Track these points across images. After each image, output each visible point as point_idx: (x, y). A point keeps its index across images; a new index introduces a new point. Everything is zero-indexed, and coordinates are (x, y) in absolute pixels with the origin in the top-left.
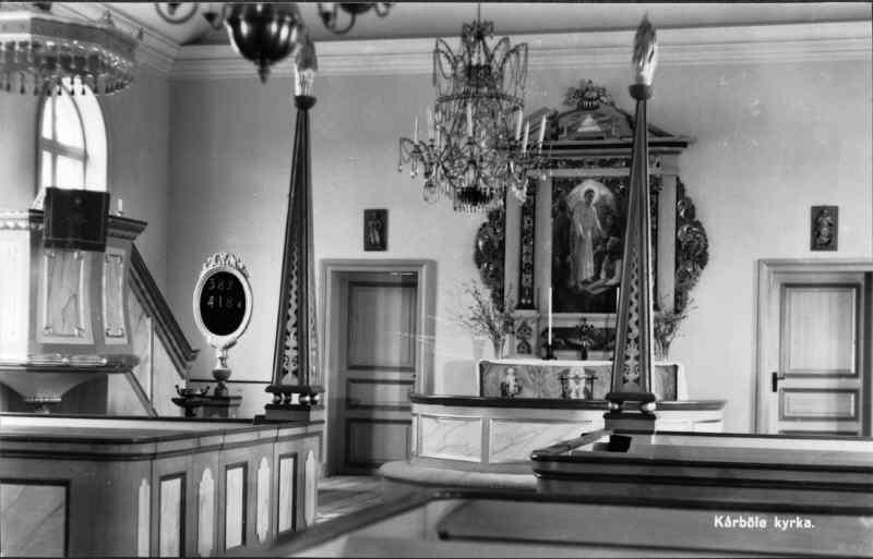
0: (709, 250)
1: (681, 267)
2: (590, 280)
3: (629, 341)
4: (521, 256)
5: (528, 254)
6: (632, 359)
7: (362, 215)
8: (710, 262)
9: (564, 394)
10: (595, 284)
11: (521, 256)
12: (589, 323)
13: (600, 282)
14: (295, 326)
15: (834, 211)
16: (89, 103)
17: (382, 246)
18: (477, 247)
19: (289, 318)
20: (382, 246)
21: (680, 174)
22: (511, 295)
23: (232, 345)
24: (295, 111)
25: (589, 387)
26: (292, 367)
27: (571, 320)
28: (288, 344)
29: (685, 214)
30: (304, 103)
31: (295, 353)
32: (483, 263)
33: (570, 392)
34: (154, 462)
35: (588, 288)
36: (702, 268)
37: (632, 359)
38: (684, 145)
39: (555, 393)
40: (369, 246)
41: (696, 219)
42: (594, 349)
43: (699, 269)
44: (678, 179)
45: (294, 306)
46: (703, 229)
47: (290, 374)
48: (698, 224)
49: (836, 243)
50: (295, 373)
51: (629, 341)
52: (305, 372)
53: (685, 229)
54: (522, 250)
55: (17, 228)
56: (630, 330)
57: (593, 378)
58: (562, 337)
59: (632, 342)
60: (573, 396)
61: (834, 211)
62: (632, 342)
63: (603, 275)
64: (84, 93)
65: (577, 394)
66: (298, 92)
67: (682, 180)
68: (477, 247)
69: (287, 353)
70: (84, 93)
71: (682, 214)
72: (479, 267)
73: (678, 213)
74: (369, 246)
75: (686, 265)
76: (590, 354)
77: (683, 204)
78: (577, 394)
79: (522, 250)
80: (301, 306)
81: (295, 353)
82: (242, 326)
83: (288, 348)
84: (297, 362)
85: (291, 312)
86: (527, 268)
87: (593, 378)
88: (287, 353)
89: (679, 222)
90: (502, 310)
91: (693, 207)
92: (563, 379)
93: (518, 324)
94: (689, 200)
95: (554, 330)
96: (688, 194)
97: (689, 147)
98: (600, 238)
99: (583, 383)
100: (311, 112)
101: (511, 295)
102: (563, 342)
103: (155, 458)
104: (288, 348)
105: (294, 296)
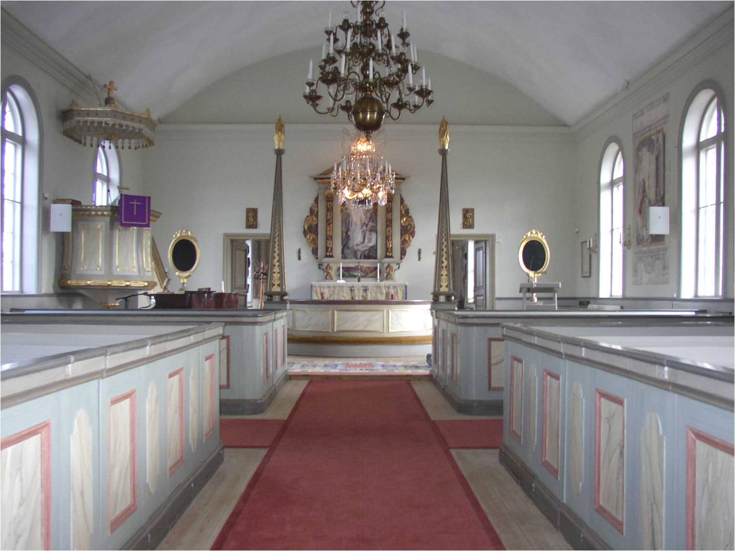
0: (415, 229)
1: (403, 237)
2: (360, 244)
3: (442, 267)
4: (327, 232)
5: (329, 231)
6: (444, 276)
7: (244, 213)
8: (416, 235)
9: (352, 298)
10: (362, 245)
11: (327, 232)
12: (361, 264)
13: (365, 244)
14: (278, 261)
15: (472, 210)
16: (112, 153)
17: (471, 226)
18: (304, 227)
19: (445, 246)
20: (471, 226)
21: (402, 194)
22: (321, 251)
23: (189, 276)
24: (275, 156)
25: (364, 294)
26: (277, 282)
27: (352, 263)
28: (274, 271)
29: (405, 213)
30: (279, 153)
31: (279, 275)
32: (307, 235)
33: (355, 296)
34: (274, 323)
35: (359, 247)
36: (413, 238)
37: (444, 276)
38: (404, 179)
39: (347, 297)
40: (249, 226)
41: (409, 215)
42: (362, 277)
43: (411, 238)
44: (401, 195)
45: (277, 252)
46: (413, 220)
47: (275, 287)
48: (411, 217)
49: (466, 228)
50: (279, 285)
51: (442, 267)
52: (284, 284)
53: (405, 219)
54: (327, 229)
55: (103, 215)
56: (443, 262)
57: (366, 289)
58: (347, 271)
59: (444, 268)
60: (357, 299)
61: (472, 210)
62: (444, 268)
63: (366, 240)
64: (110, 148)
65: (359, 297)
66: (277, 148)
67: (402, 196)
68: (304, 227)
69: (274, 275)
70: (110, 148)
71: (403, 212)
72: (305, 237)
73: (401, 212)
74: (249, 226)
75: (406, 236)
76: (361, 279)
77: (403, 207)
78: (359, 297)
79: (327, 229)
80: (281, 251)
81: (279, 275)
82: (196, 264)
83: (274, 273)
84: (280, 279)
85: (445, 249)
86: (329, 238)
87: (366, 289)
88: (274, 275)
89: (402, 217)
90: (317, 258)
91: (408, 209)
92: (352, 290)
93: (325, 265)
94: (406, 206)
95: (343, 268)
96: (405, 202)
97: (406, 180)
98: (365, 223)
99: (361, 291)
100: (283, 157)
101: (321, 251)
102: (347, 274)
103: (274, 321)
104: (274, 273)
105: (277, 247)
